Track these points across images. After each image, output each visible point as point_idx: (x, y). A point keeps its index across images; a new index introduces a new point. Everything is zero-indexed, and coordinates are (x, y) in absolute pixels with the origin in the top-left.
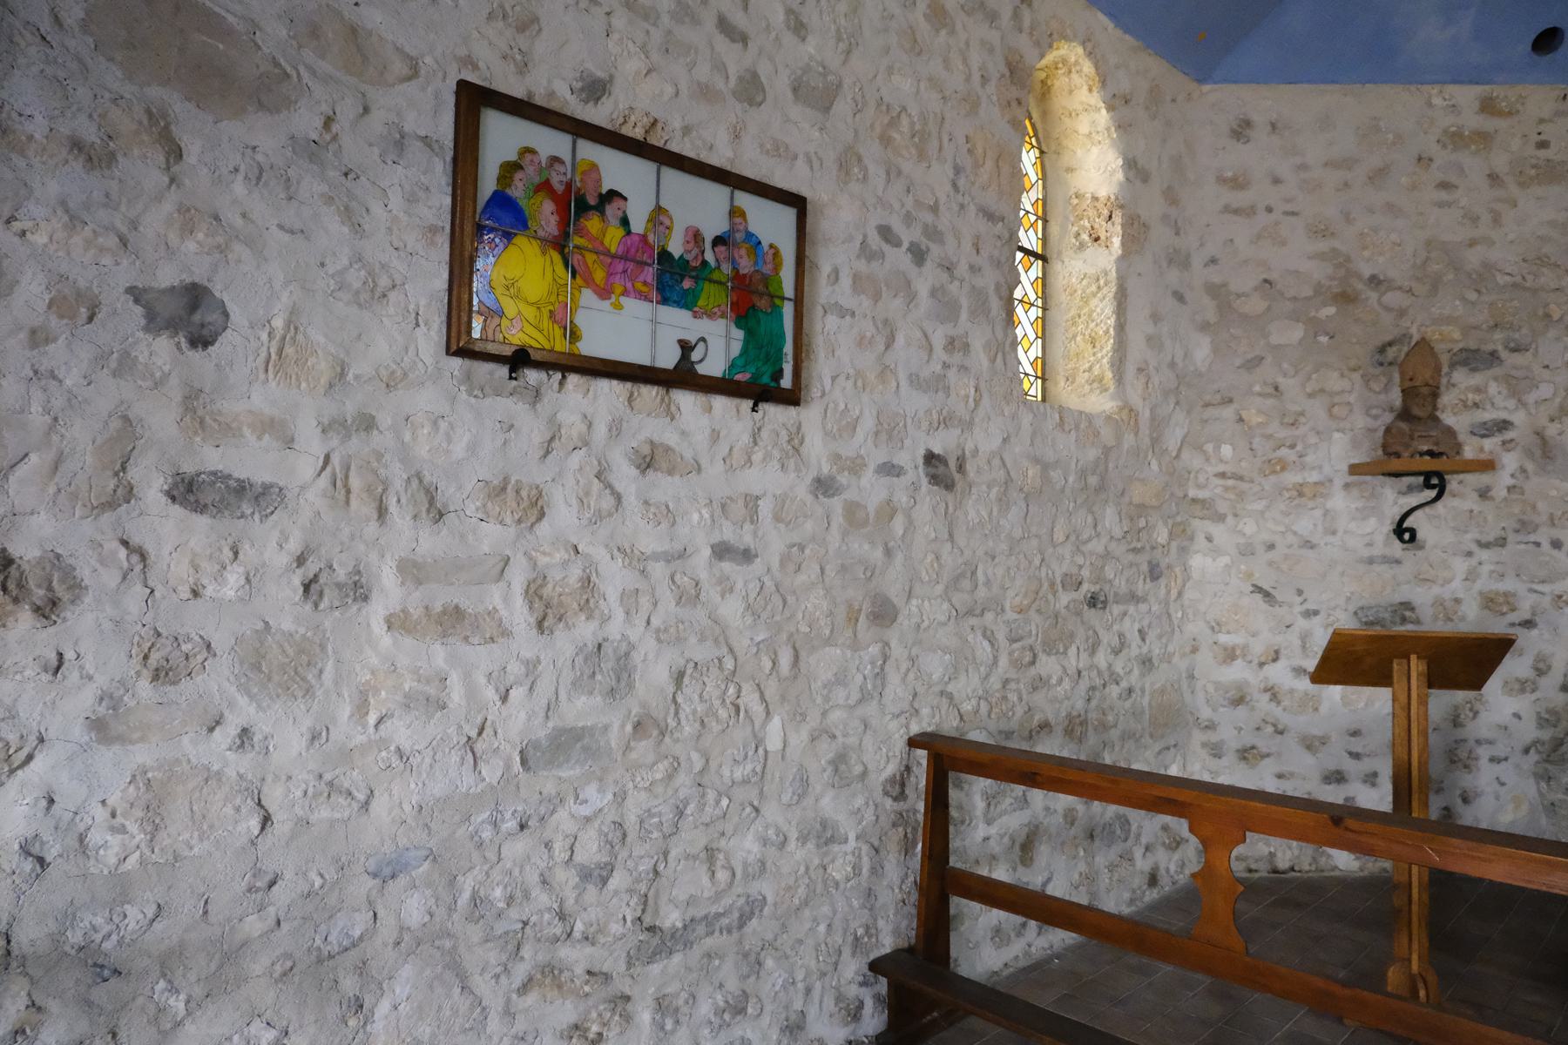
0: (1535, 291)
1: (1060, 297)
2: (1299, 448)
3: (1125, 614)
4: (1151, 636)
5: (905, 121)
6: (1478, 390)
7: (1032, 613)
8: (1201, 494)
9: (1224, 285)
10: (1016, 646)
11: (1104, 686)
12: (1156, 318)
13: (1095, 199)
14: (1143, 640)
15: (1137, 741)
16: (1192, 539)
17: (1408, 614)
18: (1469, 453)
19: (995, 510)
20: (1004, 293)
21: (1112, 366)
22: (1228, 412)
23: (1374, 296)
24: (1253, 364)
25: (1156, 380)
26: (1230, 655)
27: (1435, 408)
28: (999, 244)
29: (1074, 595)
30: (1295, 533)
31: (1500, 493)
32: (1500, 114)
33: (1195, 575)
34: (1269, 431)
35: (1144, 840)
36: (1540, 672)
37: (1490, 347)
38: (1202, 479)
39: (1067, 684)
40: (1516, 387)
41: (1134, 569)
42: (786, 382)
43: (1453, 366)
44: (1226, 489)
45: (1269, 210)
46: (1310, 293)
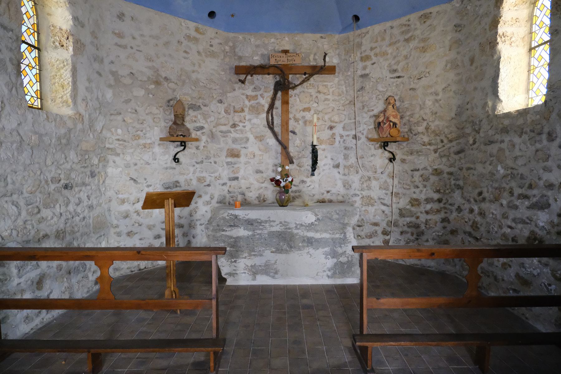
0: (210, 89)
1: (47, 67)
2: (144, 131)
3: (81, 190)
4: (92, 198)
6: (196, 117)
7: (37, 193)
8: (111, 146)
9: (117, 72)
10: (29, 207)
11: (73, 218)
12: (89, 80)
13: (61, 29)
14: (89, 199)
15: (88, 235)
16: (108, 162)
17: (178, 184)
18: (193, 136)
19: (16, 154)
20: (15, 62)
21: (71, 97)
22: (119, 118)
23: (166, 84)
24: (127, 101)
25: (90, 104)
26: (123, 202)
27: (183, 121)
28: (10, 41)
29: (57, 185)
30: (143, 160)
32: (201, 33)
33: (109, 174)
34: (134, 125)
35: (92, 270)
36: (212, 199)
37: (198, 104)
39: (55, 219)
40: (205, 116)
41: (84, 174)
43: (189, 109)
44: (120, 145)
45: (132, 48)
46: (146, 79)
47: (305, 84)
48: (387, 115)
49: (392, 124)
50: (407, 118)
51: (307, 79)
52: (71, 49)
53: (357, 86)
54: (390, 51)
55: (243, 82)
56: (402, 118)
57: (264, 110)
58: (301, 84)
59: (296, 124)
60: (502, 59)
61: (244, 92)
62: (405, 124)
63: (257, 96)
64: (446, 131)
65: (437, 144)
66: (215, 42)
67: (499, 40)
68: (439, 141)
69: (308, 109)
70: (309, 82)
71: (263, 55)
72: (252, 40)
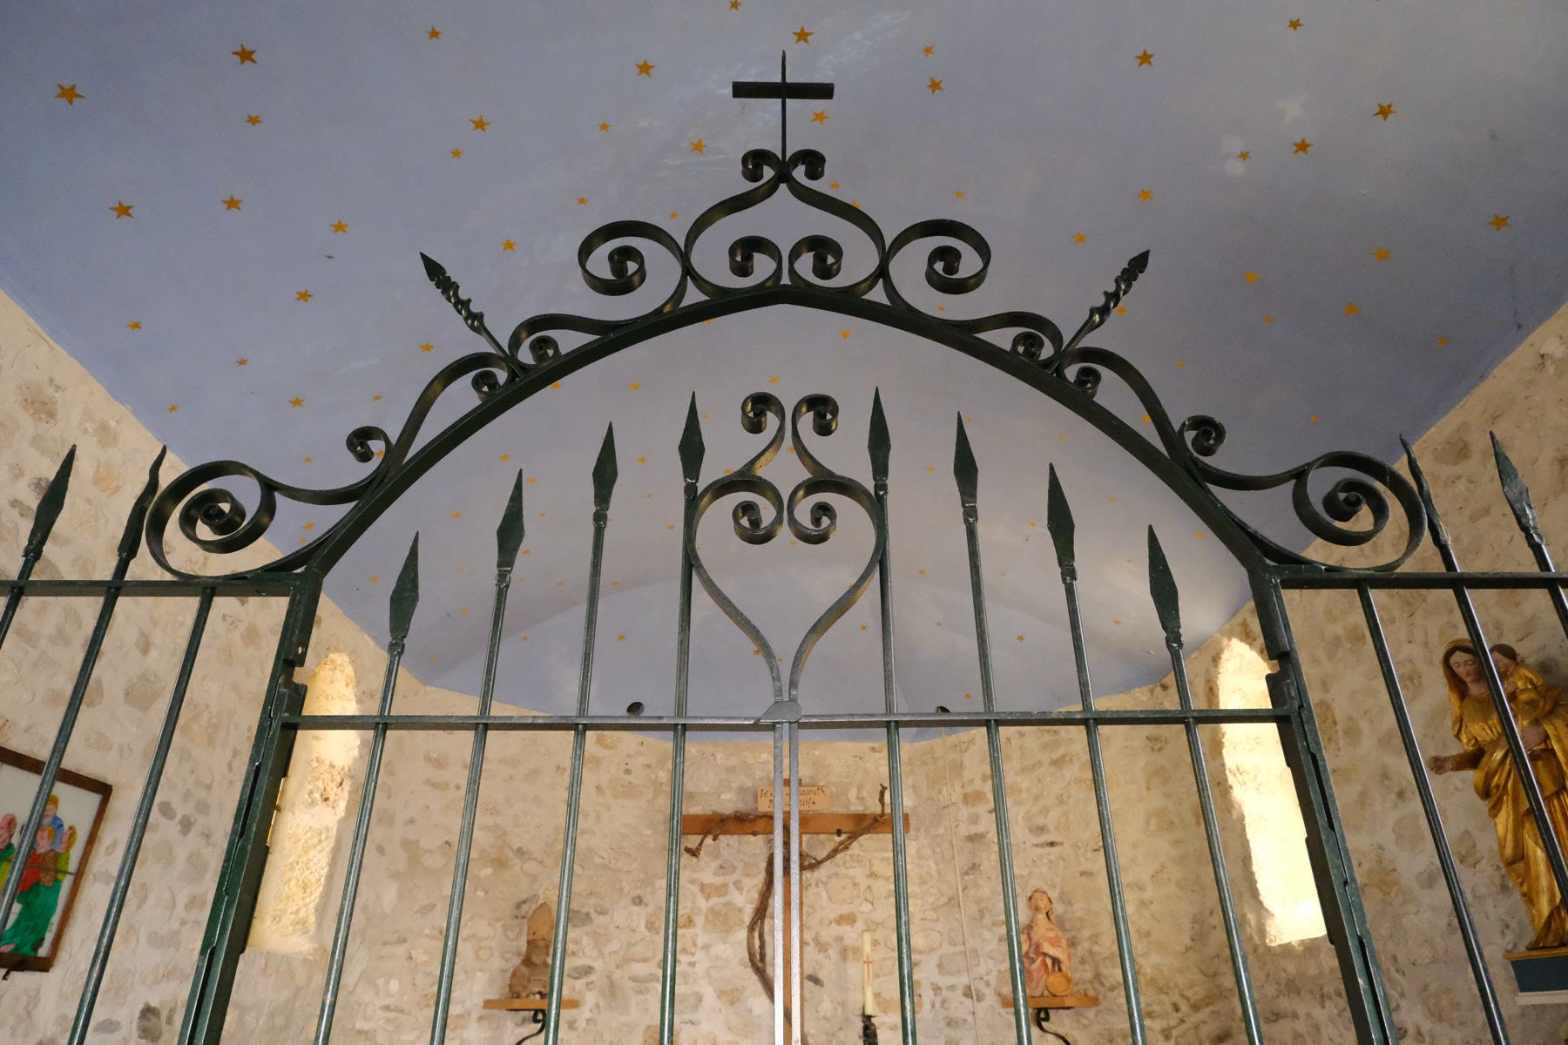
5: (205, 716)
8: (366, 1026)
13: (332, 766)
22: (401, 951)
31: (582, 1024)
37: (585, 910)
38: (369, 1012)
42: (43, 952)
44: (388, 1021)
47: (840, 856)
48: (1036, 937)
49: (1049, 962)
50: (1086, 945)
51: (844, 846)
52: (342, 805)
53: (961, 862)
54: (1024, 785)
55: (694, 853)
56: (1072, 943)
57: (742, 921)
58: (829, 857)
59: (821, 956)
60: (1247, 822)
61: (696, 875)
62: (1083, 961)
63: (725, 885)
64: (1180, 980)
65: (1164, 1016)
66: (637, 764)
67: (1231, 780)
68: (1169, 1009)
69: (850, 919)
70: (849, 852)
71: (742, 790)
72: (719, 757)
